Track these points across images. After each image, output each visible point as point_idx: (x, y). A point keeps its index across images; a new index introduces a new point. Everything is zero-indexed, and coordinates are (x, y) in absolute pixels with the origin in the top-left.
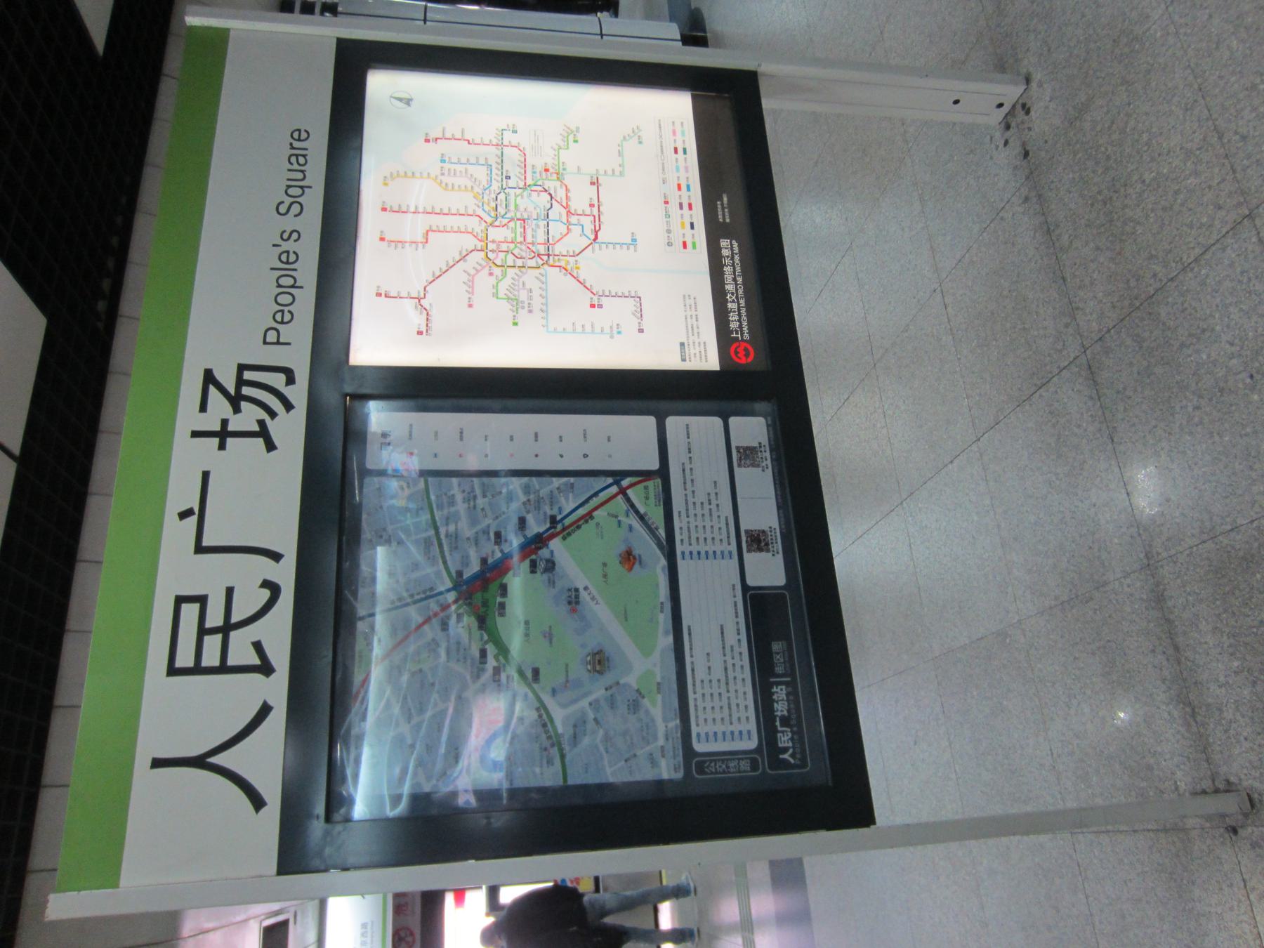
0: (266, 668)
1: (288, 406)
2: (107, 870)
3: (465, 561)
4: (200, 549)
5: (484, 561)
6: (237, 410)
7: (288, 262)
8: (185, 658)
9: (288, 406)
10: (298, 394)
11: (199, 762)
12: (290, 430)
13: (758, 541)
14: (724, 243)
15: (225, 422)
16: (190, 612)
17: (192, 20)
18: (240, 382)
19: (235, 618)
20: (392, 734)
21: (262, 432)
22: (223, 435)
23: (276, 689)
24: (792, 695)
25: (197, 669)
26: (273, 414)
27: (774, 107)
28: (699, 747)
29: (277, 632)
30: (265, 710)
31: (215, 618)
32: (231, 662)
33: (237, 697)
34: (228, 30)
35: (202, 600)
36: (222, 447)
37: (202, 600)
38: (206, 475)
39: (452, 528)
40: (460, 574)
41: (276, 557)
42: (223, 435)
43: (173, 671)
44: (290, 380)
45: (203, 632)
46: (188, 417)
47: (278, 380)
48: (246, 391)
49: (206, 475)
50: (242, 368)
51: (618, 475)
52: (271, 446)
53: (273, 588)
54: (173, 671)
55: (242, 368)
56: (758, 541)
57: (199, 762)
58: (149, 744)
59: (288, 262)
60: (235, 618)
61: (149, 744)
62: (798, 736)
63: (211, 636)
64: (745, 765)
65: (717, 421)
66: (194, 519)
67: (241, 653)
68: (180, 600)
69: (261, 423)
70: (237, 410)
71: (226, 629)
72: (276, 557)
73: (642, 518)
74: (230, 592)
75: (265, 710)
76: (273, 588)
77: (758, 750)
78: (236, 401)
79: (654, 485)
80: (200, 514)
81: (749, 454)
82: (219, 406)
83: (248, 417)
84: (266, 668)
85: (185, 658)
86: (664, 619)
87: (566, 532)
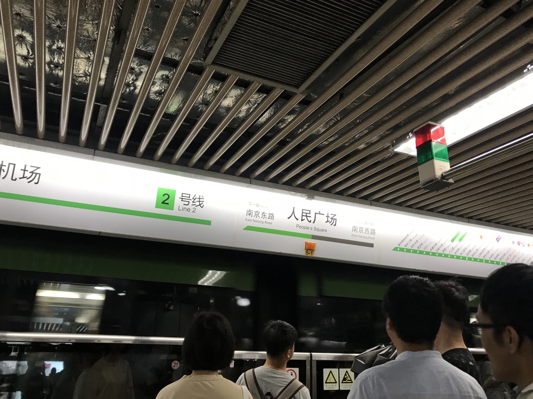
0: (302, 220)
1: (29, 182)
6: (30, 172)
8: (304, 211)
9: (29, 182)
11: (293, 212)
14: (47, 40)
16: (308, 212)
18: (36, 174)
20: (388, 287)
21: (328, 221)
22: (328, 217)
25: (303, 213)
27: (445, 129)
30: (297, 219)
31: (308, 215)
35: (310, 213)
37: (310, 213)
42: (328, 217)
44: (335, 225)
45: (307, 213)
47: (334, 224)
48: (34, 175)
49: (26, 165)
53: (310, 222)
55: (40, 174)
57: (293, 212)
67: (304, 218)
70: (30, 172)
71: (307, 216)
72: (314, 222)
78: (332, 218)
80: (319, 214)
82: (331, 216)
83: (330, 219)
84: (302, 220)
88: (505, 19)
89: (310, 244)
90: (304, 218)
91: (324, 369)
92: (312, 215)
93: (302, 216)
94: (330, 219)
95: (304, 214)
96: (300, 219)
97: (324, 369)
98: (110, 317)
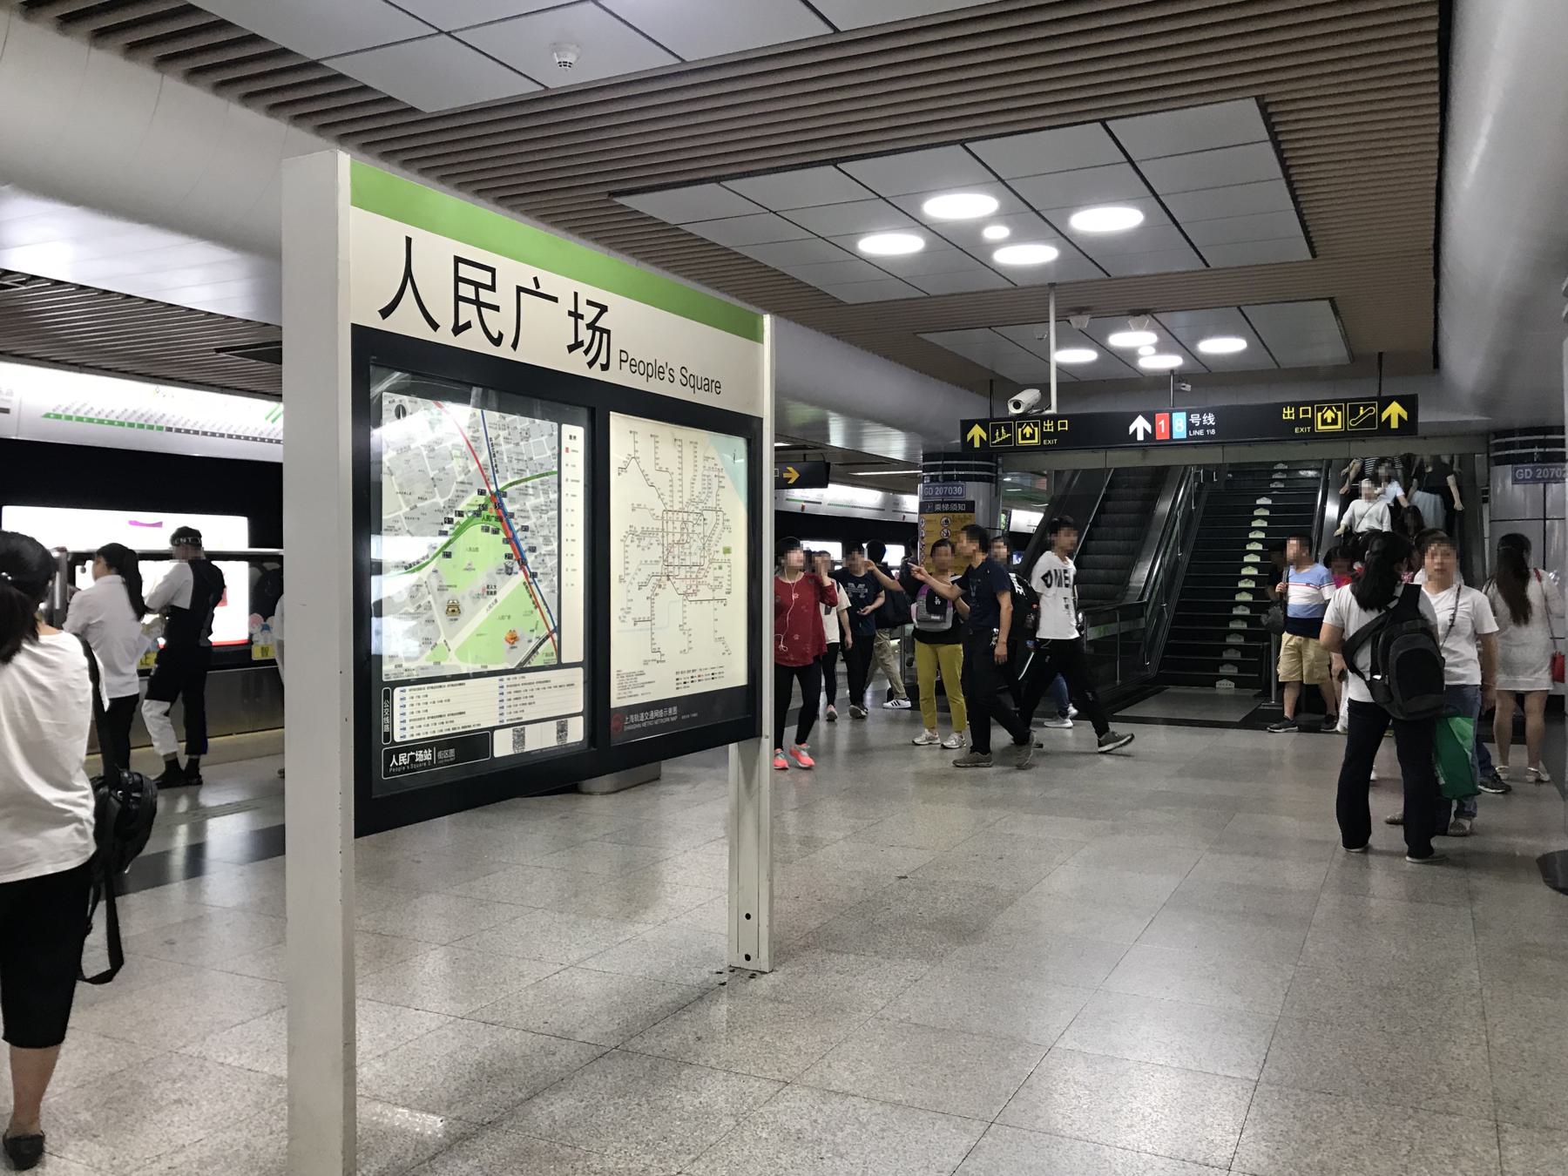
0: (457, 330)
2: (359, 200)
3: (512, 501)
4: (520, 290)
5: (512, 515)
7: (659, 372)
8: (465, 271)
9: (591, 364)
10: (595, 373)
11: (408, 273)
12: (576, 365)
13: (520, 739)
15: (582, 317)
16: (485, 278)
17: (767, 320)
18: (603, 331)
19: (483, 310)
22: (576, 315)
23: (444, 337)
24: (428, 765)
25: (458, 279)
26: (586, 352)
28: (397, 691)
29: (473, 341)
30: (435, 326)
31: (485, 296)
32: (564, 661)
33: (443, 312)
34: (762, 342)
35: (492, 288)
36: (570, 314)
37: (492, 288)
38: (555, 299)
39: (531, 491)
40: (505, 495)
41: (515, 346)
42: (576, 315)
43: (458, 260)
44: (605, 367)
46: (588, 292)
47: (602, 359)
49: (555, 299)
50: (608, 332)
51: (558, 629)
52: (571, 348)
54: (458, 260)
55: (608, 332)
56: (520, 739)
57: (408, 273)
58: (420, 237)
59: (659, 372)
60: (483, 310)
61: (420, 237)
62: (405, 769)
63: (472, 289)
64: (386, 729)
65: (580, 709)
66: (533, 288)
68: (493, 271)
69: (581, 344)
73: (534, 651)
74: (497, 308)
75: (435, 326)
76: (497, 341)
77: (394, 743)
79: (553, 660)
81: (562, 730)
82: (590, 313)
83: (585, 335)
84: (457, 330)
85: (465, 271)
86: (478, 668)
87: (527, 585)
88: (1406, 847)
89: (1559, 684)
90: (468, 312)
91: (5, 509)
92: (504, 296)
93: (458, 298)
94: (585, 335)
95: (467, 291)
96: (447, 323)
97: (5, 509)
98: (679, 715)
